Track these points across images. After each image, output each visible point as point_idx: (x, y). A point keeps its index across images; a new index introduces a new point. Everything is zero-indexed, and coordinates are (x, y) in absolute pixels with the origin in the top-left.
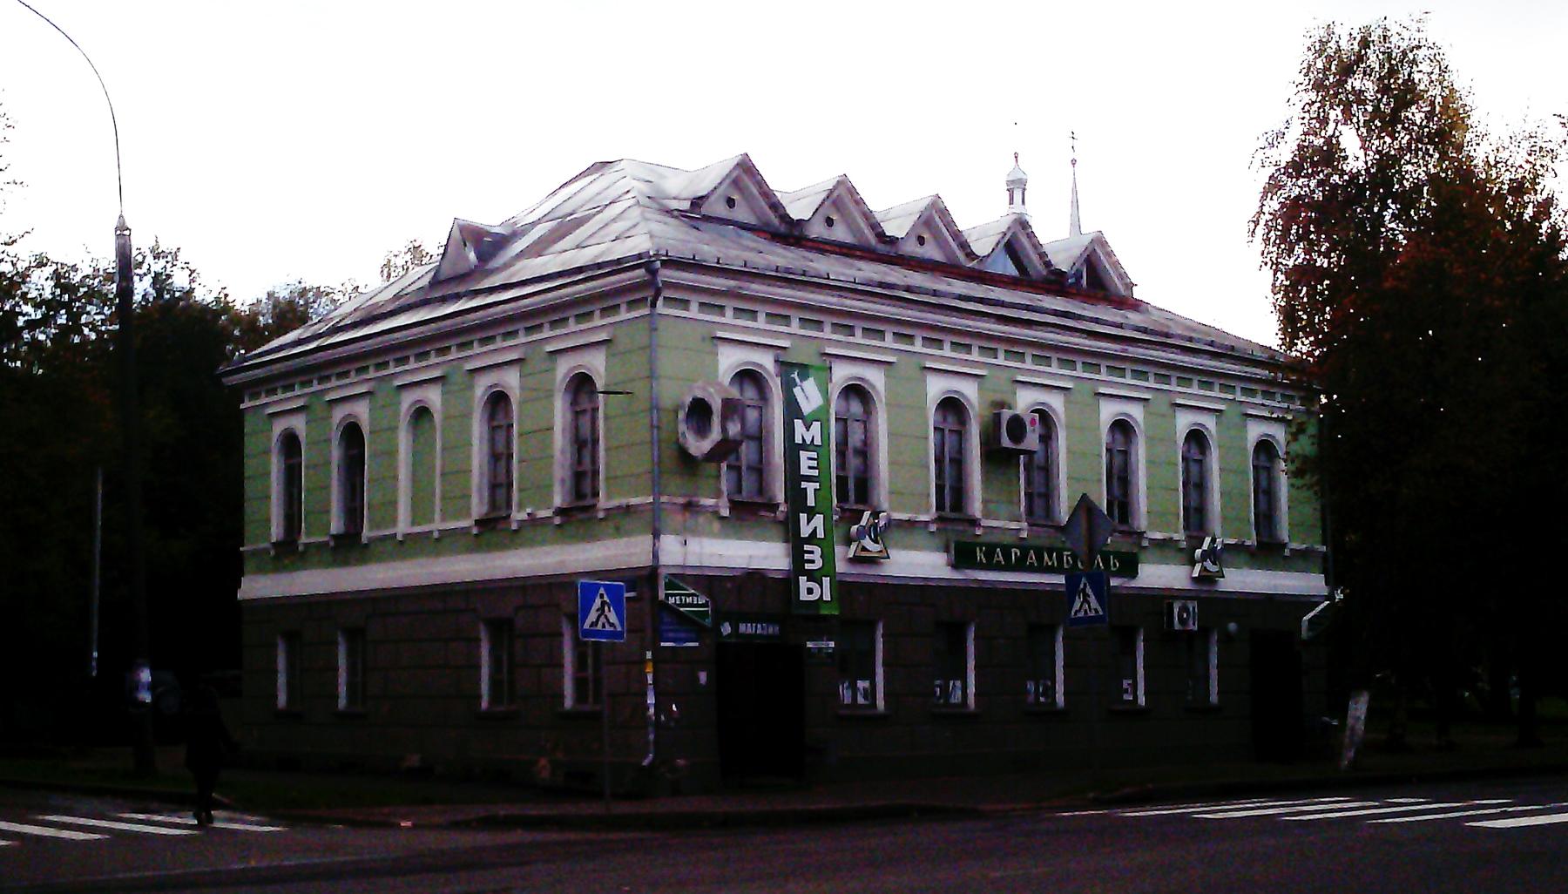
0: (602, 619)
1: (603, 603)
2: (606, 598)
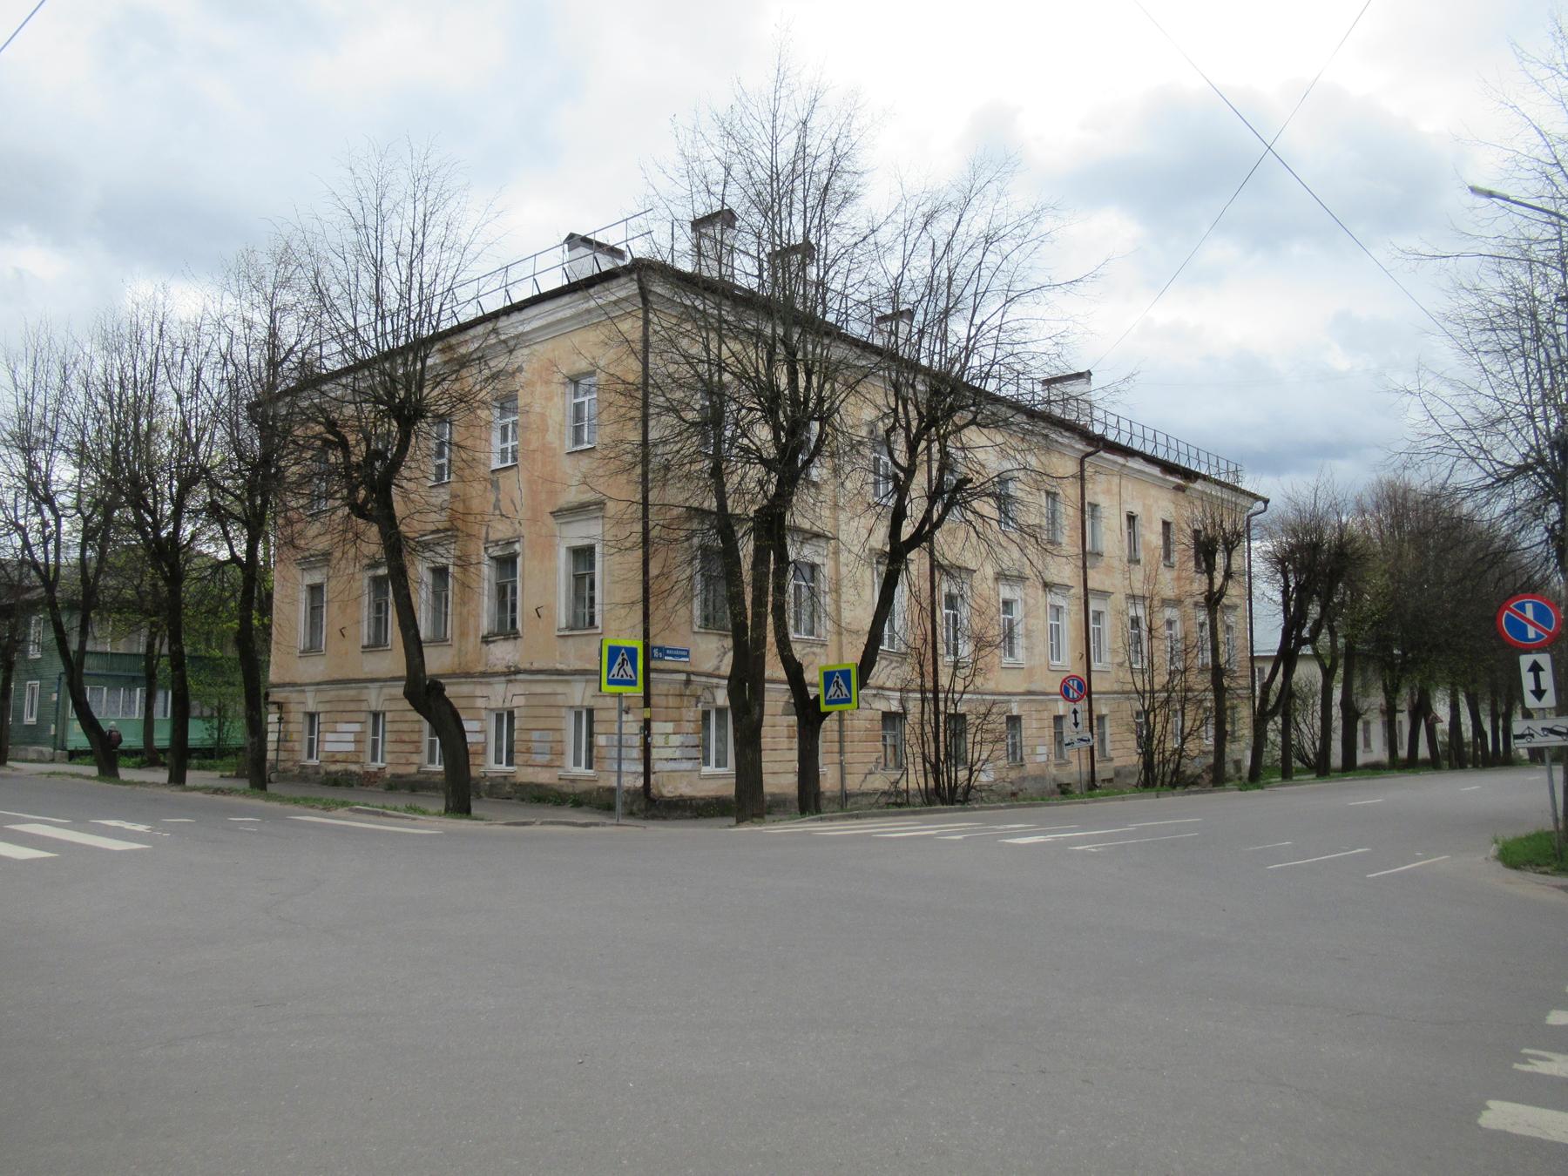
0: (622, 672)
1: (623, 660)
2: (625, 656)
